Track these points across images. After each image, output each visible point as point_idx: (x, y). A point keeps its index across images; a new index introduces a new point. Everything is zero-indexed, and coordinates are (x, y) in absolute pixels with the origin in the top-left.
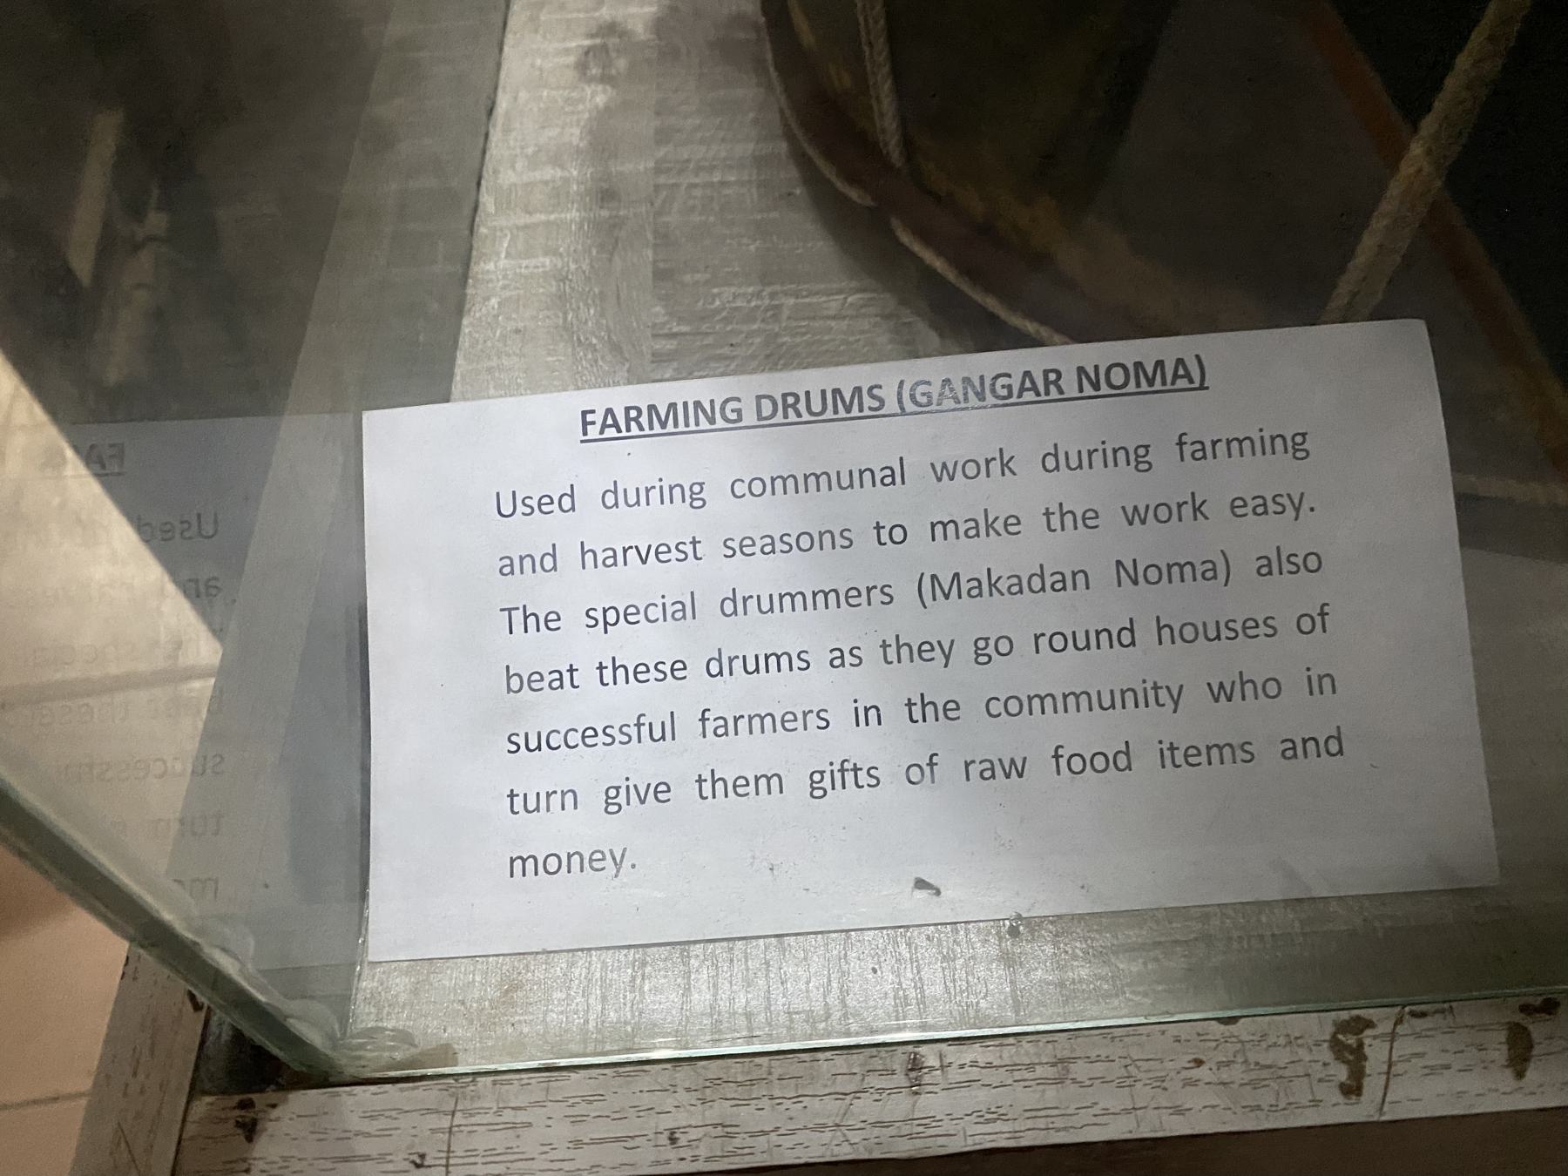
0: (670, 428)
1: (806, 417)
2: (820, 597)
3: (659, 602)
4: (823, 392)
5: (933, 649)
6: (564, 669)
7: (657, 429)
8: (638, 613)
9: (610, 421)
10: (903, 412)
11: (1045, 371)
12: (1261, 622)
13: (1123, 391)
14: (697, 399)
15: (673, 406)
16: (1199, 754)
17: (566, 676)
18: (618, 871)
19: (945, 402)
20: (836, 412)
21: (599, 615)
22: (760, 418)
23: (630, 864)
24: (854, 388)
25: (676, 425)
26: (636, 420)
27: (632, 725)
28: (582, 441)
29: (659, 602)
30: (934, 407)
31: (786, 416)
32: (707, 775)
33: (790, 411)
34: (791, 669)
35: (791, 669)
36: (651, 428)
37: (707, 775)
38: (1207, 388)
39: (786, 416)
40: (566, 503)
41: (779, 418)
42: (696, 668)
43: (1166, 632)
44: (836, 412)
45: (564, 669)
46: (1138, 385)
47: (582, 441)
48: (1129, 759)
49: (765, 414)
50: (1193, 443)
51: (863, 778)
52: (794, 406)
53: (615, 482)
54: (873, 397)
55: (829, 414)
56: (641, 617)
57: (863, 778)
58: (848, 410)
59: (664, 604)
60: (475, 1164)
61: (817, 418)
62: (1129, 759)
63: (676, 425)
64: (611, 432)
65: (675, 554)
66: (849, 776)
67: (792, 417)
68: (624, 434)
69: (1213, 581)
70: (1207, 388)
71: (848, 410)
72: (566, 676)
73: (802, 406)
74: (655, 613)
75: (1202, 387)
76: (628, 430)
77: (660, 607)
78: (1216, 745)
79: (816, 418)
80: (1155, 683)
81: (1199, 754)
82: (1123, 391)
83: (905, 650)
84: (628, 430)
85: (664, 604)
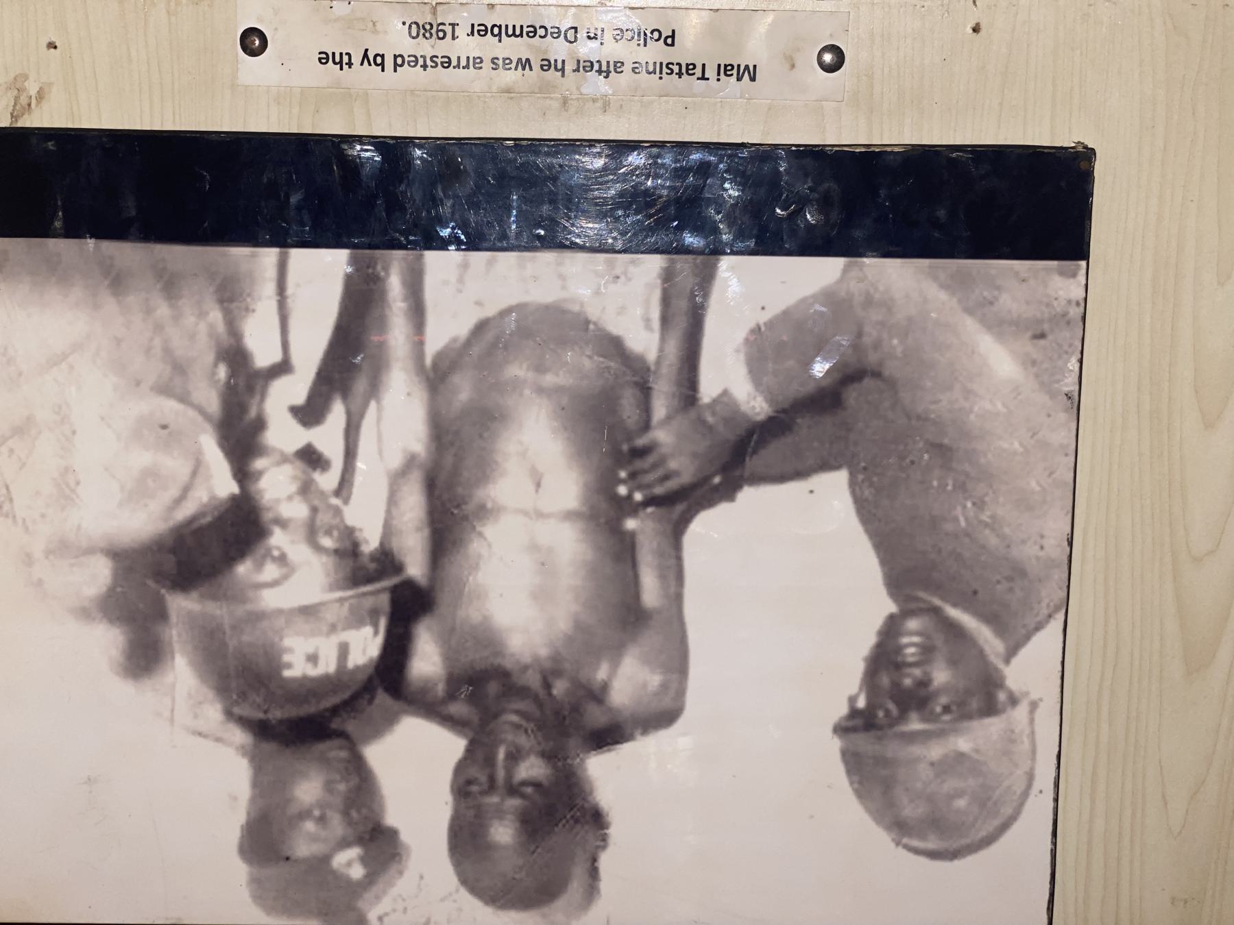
11: (383, 55)
14: (753, 83)
16: (479, 31)
17: (684, 70)
24: (741, 80)
27: (429, 67)
32: (345, 67)
37: (345, 67)
38: (708, 79)
40: (399, 61)
42: (536, 65)
43: (559, 66)
50: (442, 57)
51: (676, 69)
54: (496, 64)
57: (676, 69)
60: (482, 30)
65: (439, 61)
66: (604, 68)
69: (689, 63)
70: (708, 79)
72: (684, 70)
78: (517, 36)
80: (680, 77)
81: (479, 31)
83: (337, 60)
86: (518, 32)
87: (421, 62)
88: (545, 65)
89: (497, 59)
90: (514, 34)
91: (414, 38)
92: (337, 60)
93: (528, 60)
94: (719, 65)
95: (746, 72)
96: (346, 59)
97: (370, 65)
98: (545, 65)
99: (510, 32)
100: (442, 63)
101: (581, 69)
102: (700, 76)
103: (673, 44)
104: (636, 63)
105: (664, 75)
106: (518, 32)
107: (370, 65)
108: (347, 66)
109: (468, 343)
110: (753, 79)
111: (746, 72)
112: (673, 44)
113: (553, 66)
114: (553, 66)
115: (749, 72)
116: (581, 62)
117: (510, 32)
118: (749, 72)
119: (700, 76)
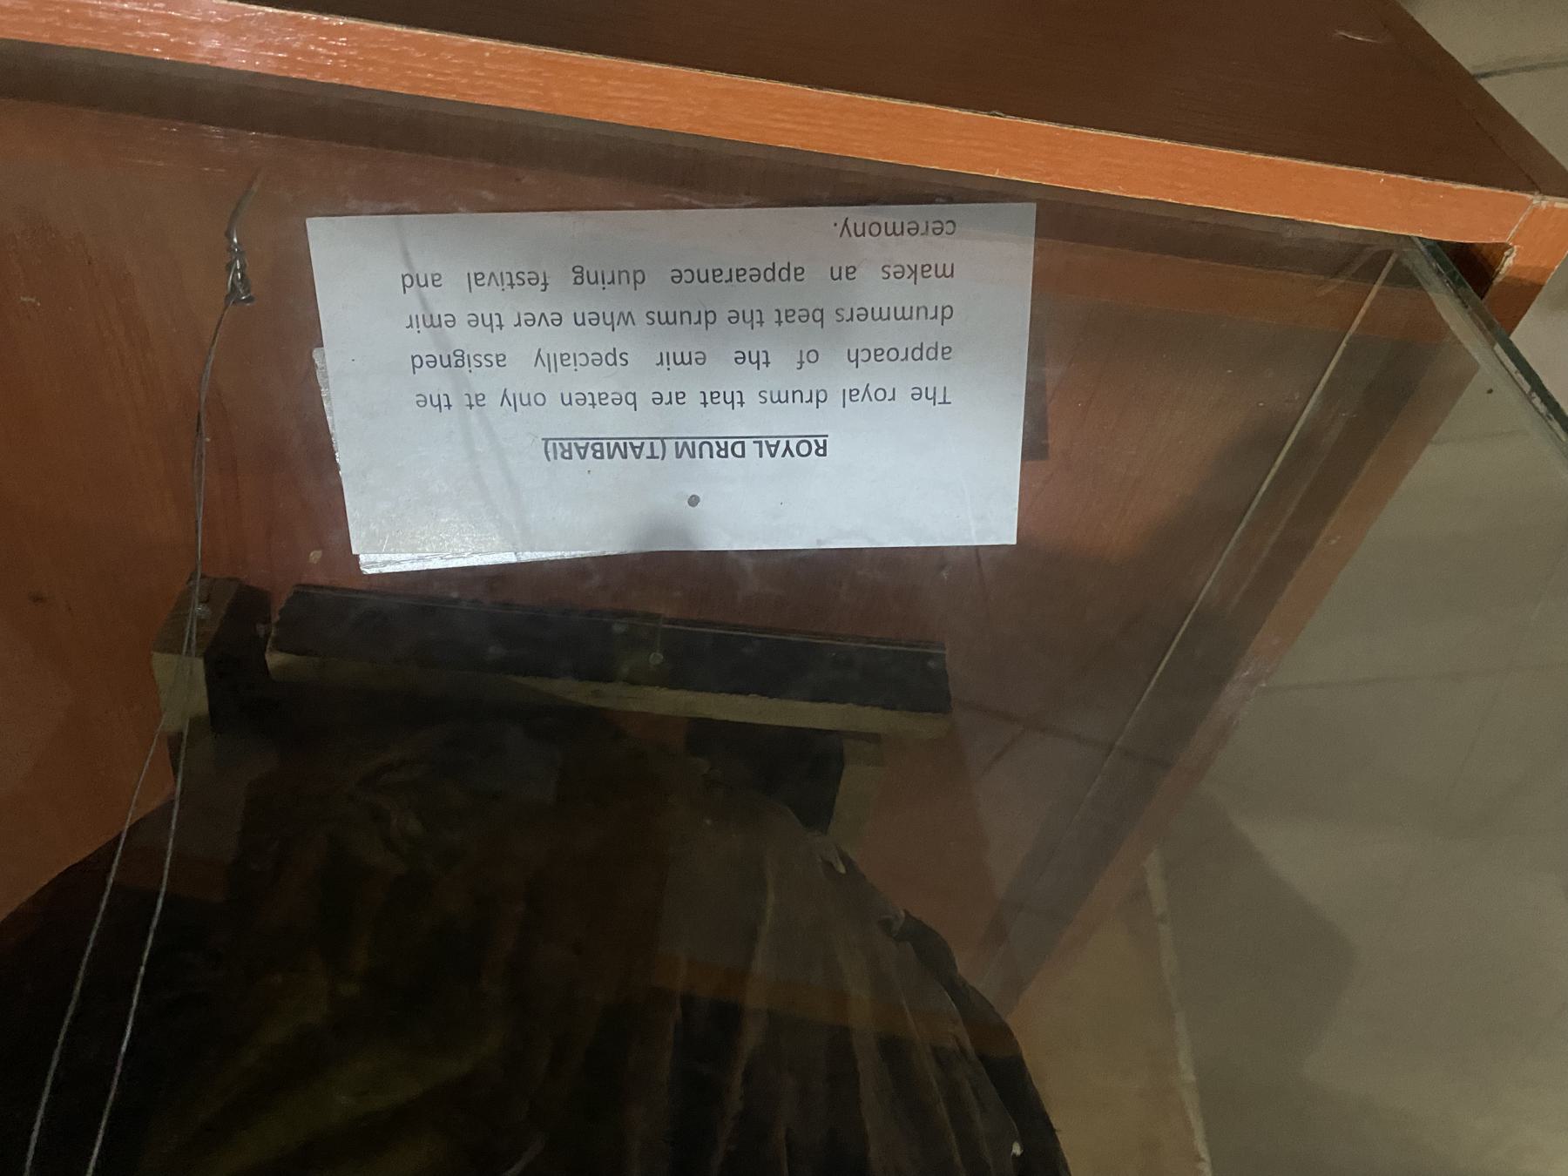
0: (612, 443)
1: (713, 442)
2: (885, 316)
3: (578, 367)
4: (701, 456)
5: (552, 320)
6: (785, 323)
7: (621, 443)
8: (593, 360)
9: (638, 450)
10: (662, 439)
12: (527, 282)
13: (738, 440)
14: (694, 459)
15: (611, 457)
18: (846, 222)
19: (639, 445)
20: (693, 443)
21: (619, 361)
22: (743, 443)
23: (838, 226)
25: (608, 444)
26: (819, 447)
28: (827, 436)
29: (578, 367)
30: (591, 442)
31: (726, 443)
33: (723, 446)
34: (659, 313)
35: (659, 313)
36: (625, 444)
37: (757, 326)
38: (543, 439)
39: (726, 443)
41: (731, 442)
42: (723, 316)
44: (693, 443)
45: (785, 323)
46: (693, 443)
47: (827, 436)
48: (404, 283)
49: (739, 446)
52: (819, 447)
53: (817, 407)
55: (697, 443)
56: (591, 357)
58: (685, 444)
59: (575, 365)
61: (706, 441)
62: (404, 283)
63: (608, 444)
64: (637, 443)
65: (525, 277)
67: (722, 442)
68: (573, 442)
69: (739, 268)
70: (543, 439)
71: (685, 444)
73: (716, 449)
74: (582, 360)
75: (546, 440)
76: (570, 444)
77: (578, 363)
79: (708, 440)
82: (738, 440)
84: (570, 444)
85: (575, 365)
87: (589, 400)
88: (533, 279)
92: (487, 322)
95: (617, 449)
96: (496, 321)
98: (533, 279)
100: (529, 280)
102: (649, 455)
103: (825, 455)
104: (948, 359)
108: (759, 325)
111: (617, 449)
112: (825, 455)
115: (620, 450)
116: (573, 395)
118: (620, 450)
119: (649, 455)
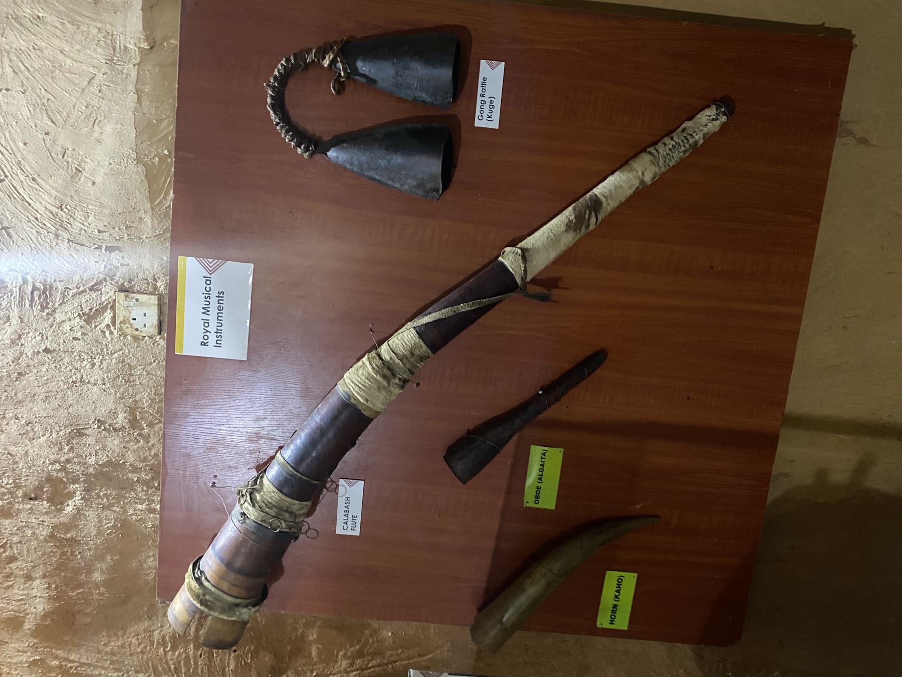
16: (220, 306)
78: (218, 317)
81: (220, 306)
86: (219, 318)
89: (209, 299)
90: (218, 316)
91: (222, 326)
93: (613, 624)
94: (209, 320)
97: (204, 333)
99: (219, 315)
101: (219, 305)
103: (201, 345)
105: (205, 295)
106: (219, 318)
107: (204, 333)
109: (287, 80)
110: (610, 623)
112: (201, 345)
113: (220, 312)
114: (220, 312)
117: (219, 315)
